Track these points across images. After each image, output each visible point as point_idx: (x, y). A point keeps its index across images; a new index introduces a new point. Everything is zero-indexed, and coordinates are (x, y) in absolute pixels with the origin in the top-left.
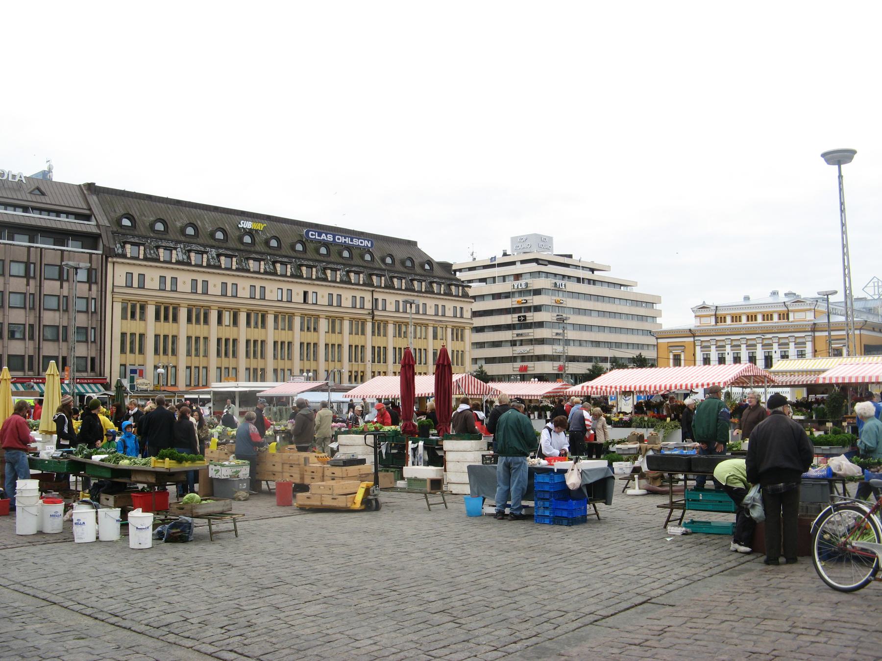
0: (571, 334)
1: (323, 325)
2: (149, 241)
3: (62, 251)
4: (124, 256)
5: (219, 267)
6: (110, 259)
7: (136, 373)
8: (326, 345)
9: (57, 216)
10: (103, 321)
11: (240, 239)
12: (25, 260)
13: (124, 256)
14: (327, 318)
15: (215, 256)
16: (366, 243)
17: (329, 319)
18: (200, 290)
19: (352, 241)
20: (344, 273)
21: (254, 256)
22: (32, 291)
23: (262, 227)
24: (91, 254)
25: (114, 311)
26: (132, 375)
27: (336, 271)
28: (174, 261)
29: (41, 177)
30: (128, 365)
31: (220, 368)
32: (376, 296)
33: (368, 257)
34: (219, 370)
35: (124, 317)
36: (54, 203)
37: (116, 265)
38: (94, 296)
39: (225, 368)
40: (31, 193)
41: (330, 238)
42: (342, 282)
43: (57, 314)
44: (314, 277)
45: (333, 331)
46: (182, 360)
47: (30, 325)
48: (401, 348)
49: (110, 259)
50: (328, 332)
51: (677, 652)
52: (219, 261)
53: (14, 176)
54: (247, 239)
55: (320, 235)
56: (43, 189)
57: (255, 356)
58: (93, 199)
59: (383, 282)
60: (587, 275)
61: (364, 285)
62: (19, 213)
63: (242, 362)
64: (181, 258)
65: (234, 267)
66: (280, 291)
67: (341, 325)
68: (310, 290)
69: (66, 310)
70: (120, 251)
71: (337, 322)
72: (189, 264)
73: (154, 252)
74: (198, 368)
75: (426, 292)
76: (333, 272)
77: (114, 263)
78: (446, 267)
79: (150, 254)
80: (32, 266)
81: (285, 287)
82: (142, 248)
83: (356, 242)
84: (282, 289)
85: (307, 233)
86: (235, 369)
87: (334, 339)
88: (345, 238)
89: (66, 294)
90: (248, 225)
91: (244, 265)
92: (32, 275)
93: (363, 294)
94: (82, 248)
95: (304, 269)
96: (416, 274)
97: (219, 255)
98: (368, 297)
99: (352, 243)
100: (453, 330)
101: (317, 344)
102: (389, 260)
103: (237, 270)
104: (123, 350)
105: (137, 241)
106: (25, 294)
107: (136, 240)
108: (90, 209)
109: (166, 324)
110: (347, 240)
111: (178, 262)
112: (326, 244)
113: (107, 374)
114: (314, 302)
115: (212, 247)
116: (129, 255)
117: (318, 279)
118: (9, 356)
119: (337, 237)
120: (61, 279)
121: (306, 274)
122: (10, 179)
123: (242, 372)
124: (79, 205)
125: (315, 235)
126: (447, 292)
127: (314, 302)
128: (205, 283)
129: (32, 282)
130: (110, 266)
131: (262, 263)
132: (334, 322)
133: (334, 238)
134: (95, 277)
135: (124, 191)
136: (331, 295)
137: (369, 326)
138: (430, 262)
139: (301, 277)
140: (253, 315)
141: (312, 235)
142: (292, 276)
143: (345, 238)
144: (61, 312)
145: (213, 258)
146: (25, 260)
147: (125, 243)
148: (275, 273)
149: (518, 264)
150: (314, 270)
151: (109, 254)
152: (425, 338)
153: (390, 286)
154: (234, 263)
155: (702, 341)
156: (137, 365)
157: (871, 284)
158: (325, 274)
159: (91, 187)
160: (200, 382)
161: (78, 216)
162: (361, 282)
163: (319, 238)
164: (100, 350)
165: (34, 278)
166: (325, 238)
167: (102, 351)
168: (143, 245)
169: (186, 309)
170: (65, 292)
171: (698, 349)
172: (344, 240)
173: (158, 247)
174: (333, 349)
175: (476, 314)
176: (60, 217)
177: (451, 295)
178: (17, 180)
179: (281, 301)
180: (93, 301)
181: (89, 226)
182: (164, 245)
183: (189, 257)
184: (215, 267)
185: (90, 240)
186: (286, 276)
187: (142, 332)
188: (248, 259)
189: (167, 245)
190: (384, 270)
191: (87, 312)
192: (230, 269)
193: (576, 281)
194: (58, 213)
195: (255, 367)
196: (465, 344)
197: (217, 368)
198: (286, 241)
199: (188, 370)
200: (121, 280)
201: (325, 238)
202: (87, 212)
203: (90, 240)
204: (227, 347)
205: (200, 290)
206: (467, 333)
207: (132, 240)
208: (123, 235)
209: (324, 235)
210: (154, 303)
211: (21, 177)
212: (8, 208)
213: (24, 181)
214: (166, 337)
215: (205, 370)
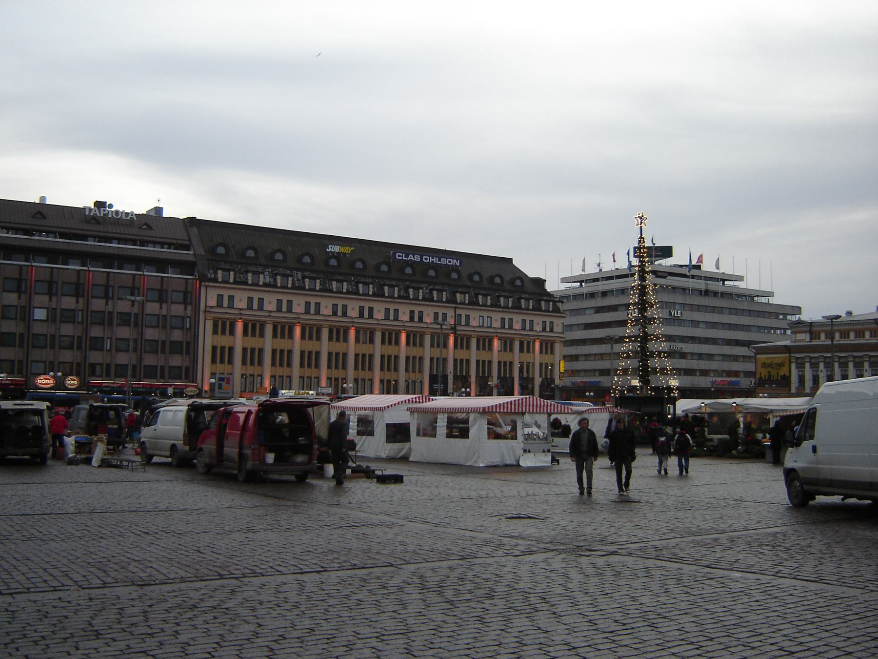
2: (240, 267)
3: (162, 277)
4: (215, 280)
5: (303, 288)
6: (203, 283)
7: (224, 381)
8: (406, 357)
10: (196, 337)
11: (326, 263)
12: (159, 287)
13: (215, 280)
14: (500, 339)
15: (300, 278)
16: (455, 262)
17: (501, 340)
19: (439, 260)
20: (428, 291)
22: (23, 304)
23: (350, 250)
25: (206, 328)
26: (220, 382)
27: (229, 272)
28: (261, 283)
29: (153, 214)
30: (218, 373)
31: (303, 377)
32: (458, 312)
33: (454, 275)
34: (301, 379)
35: (215, 332)
36: (162, 236)
37: (209, 289)
38: (189, 315)
39: (362, 379)
40: (33, 217)
41: (417, 258)
42: (424, 299)
43: (157, 330)
44: (396, 295)
45: (505, 350)
47: (51, 335)
48: (416, 357)
49: (203, 283)
50: (501, 351)
52: (304, 283)
53: (127, 214)
54: (333, 262)
55: (407, 256)
57: (389, 370)
58: (194, 230)
59: (467, 298)
61: (448, 301)
63: (296, 371)
64: (267, 281)
65: (318, 288)
66: (481, 318)
68: (417, 309)
69: (164, 327)
72: (275, 286)
73: (244, 277)
74: (364, 380)
75: (513, 308)
76: (365, 286)
77: (206, 287)
79: (240, 278)
81: (485, 314)
83: (444, 261)
84: (483, 317)
85: (394, 254)
86: (290, 377)
88: (433, 258)
90: (335, 249)
91: (327, 285)
93: (445, 311)
94: (181, 274)
96: (505, 291)
97: (304, 278)
98: (450, 313)
99: (440, 262)
101: (346, 353)
102: (476, 278)
103: (321, 290)
104: (213, 361)
105: (228, 267)
106: (158, 316)
107: (527, 296)
108: (190, 240)
109: (390, 346)
110: (434, 260)
111: (265, 285)
112: (411, 264)
114: (489, 325)
115: (298, 270)
117: (399, 297)
118: (116, 365)
119: (424, 257)
120: (185, 303)
121: (504, 303)
122: (124, 217)
123: (296, 381)
125: (402, 256)
126: (536, 307)
127: (489, 325)
128: (290, 302)
129: (23, 296)
130: (203, 290)
131: (345, 284)
133: (421, 258)
134: (190, 298)
135: (192, 221)
139: (383, 295)
140: (307, 329)
141: (399, 256)
142: (374, 295)
143: (433, 258)
144: (106, 325)
145: (298, 280)
146: (17, 276)
147: (218, 269)
150: (396, 289)
151: (203, 278)
153: (474, 303)
154: (318, 284)
155: (840, 357)
156: (226, 373)
158: (408, 292)
160: (247, 389)
162: (531, 308)
163: (440, 262)
164: (194, 361)
165: (25, 293)
166: (412, 258)
167: (195, 362)
168: (233, 270)
169: (381, 332)
170: (164, 312)
172: (431, 260)
173: (247, 272)
175: (569, 327)
177: (540, 310)
178: (129, 218)
179: (483, 326)
180: (80, 313)
181: (186, 255)
182: (252, 270)
183: (275, 280)
185: (187, 267)
186: (368, 295)
188: (332, 280)
189: (255, 269)
190: (470, 287)
191: (182, 328)
192: (314, 290)
193: (712, 295)
195: (389, 379)
196: (514, 355)
197: (300, 377)
198: (486, 275)
199: (273, 379)
200: (212, 302)
201: (412, 258)
202: (188, 243)
203: (187, 267)
204: (310, 359)
205: (528, 328)
206: (558, 347)
208: (215, 261)
209: (411, 255)
210: (328, 326)
211: (132, 215)
212: (157, 246)
213: (135, 219)
214: (389, 357)
215: (288, 379)
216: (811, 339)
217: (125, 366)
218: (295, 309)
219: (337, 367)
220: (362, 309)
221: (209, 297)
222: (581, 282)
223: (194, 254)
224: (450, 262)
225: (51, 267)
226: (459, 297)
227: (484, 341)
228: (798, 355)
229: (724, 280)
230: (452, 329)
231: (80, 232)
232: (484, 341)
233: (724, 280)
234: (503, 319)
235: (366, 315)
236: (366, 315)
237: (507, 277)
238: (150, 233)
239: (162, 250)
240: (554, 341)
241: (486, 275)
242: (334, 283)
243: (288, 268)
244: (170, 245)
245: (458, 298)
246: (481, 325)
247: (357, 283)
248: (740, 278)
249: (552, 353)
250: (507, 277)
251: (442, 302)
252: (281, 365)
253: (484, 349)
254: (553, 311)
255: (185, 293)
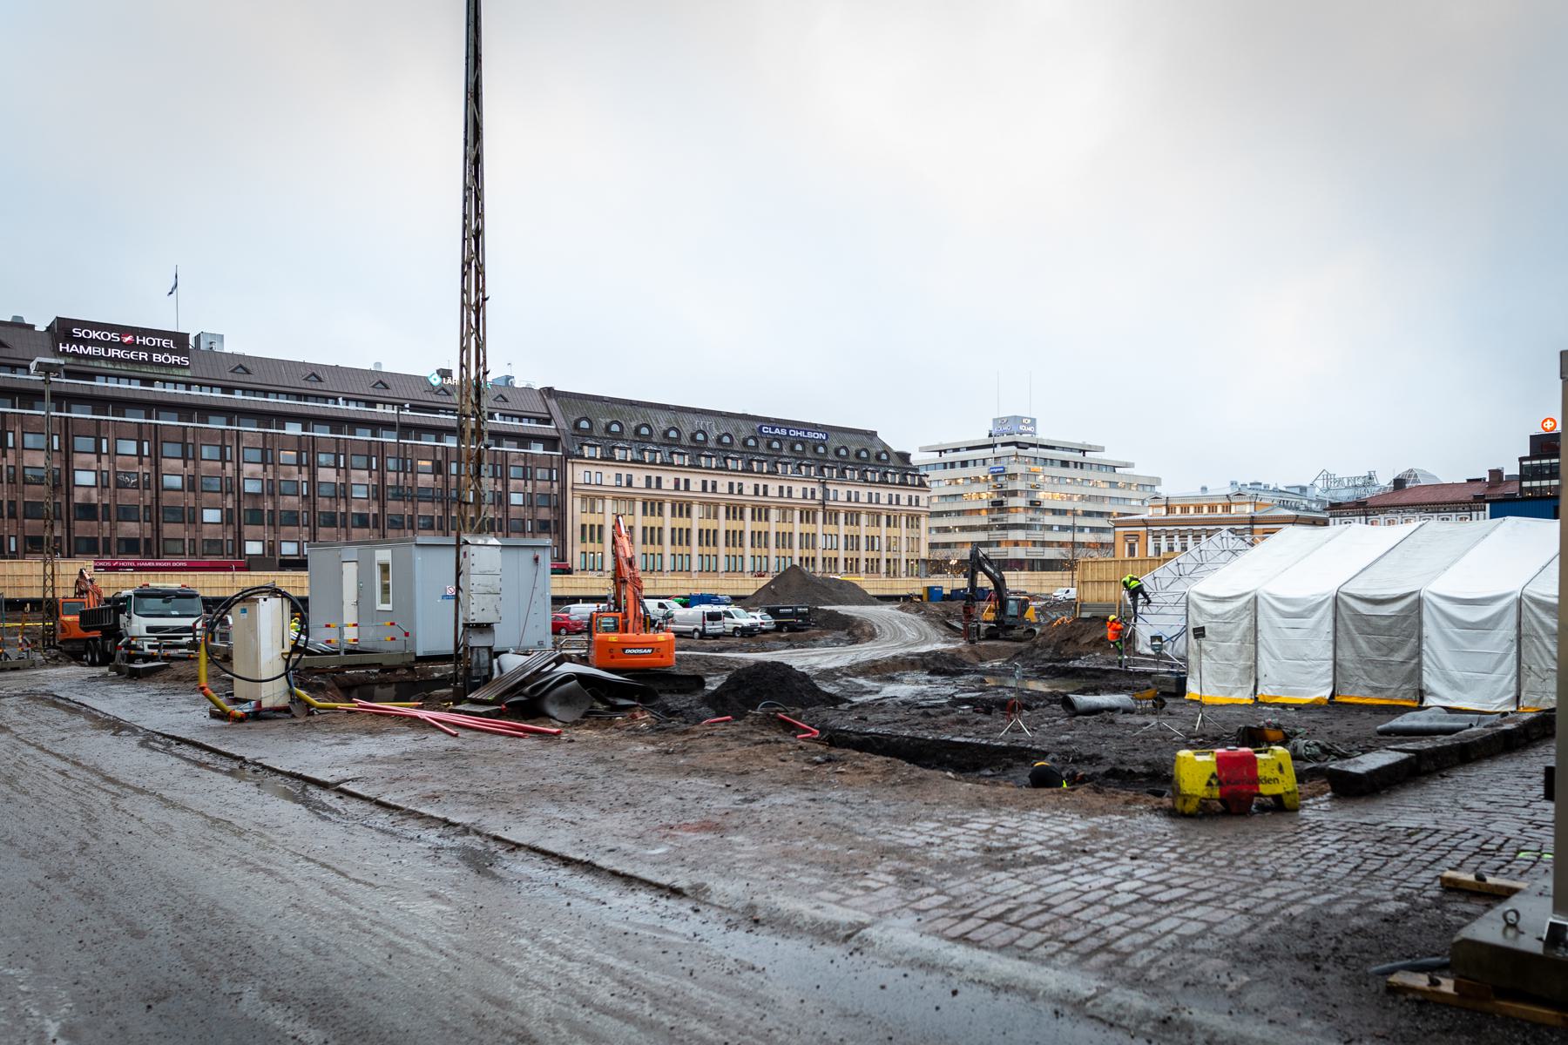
0: (1049, 519)
1: (774, 514)
4: (582, 457)
9: (520, 421)
10: (564, 514)
12: (181, 439)
13: (582, 457)
18: (874, 501)
21: (732, 455)
24: (265, 433)
28: (629, 459)
31: (646, 554)
33: (821, 450)
40: (495, 400)
41: (784, 432)
45: (708, 517)
46: (668, 548)
51: (1074, 885)
55: (773, 430)
56: (506, 396)
58: (553, 403)
60: (1078, 457)
62: (516, 422)
64: (635, 457)
67: (793, 514)
70: (578, 453)
71: (789, 512)
78: (904, 457)
80: (228, 449)
82: (599, 449)
83: (810, 435)
85: (761, 427)
87: (785, 528)
89: (271, 477)
92: (228, 458)
94: (93, 414)
95: (755, 463)
100: (801, 513)
103: (690, 466)
108: (550, 414)
111: (633, 461)
112: (778, 438)
113: (569, 562)
116: (586, 456)
120: (525, 478)
124: (540, 409)
130: (569, 466)
132: (785, 511)
136: (870, 494)
137: (820, 515)
138: (887, 450)
139: (752, 471)
148: (726, 469)
149: (999, 446)
151: (568, 455)
152: (792, 522)
154: (687, 460)
157: (1321, 477)
159: (549, 392)
161: (539, 421)
165: (231, 461)
171: (1150, 538)
174: (681, 536)
176: (190, 390)
181: (548, 430)
184: (721, 469)
185: (551, 442)
187: (715, 528)
194: (266, 393)
202: (548, 416)
205: (874, 501)
206: (923, 520)
207: (590, 442)
214: (681, 530)
216: (1168, 513)
217: (136, 541)
218: (664, 485)
219: (807, 548)
220: (677, 482)
221: (578, 474)
222: (940, 452)
223: (557, 429)
224: (167, 359)
225: (97, 420)
226: (618, 454)
227: (808, 513)
228: (1154, 529)
229: (1084, 451)
230: (820, 504)
231: (420, 403)
232: (808, 513)
233: (1084, 451)
234: (870, 494)
235: (761, 493)
236: (761, 493)
237: (873, 451)
238: (319, 386)
239: (14, 376)
240: (860, 512)
241: (853, 449)
242: (703, 459)
243: (655, 444)
244: (288, 395)
245: (617, 454)
246: (587, 481)
247: (725, 459)
248: (1102, 449)
249: (767, 519)
250: (873, 451)
251: (762, 473)
252: (652, 542)
253: (808, 521)
254: (919, 485)
255: (264, 451)
